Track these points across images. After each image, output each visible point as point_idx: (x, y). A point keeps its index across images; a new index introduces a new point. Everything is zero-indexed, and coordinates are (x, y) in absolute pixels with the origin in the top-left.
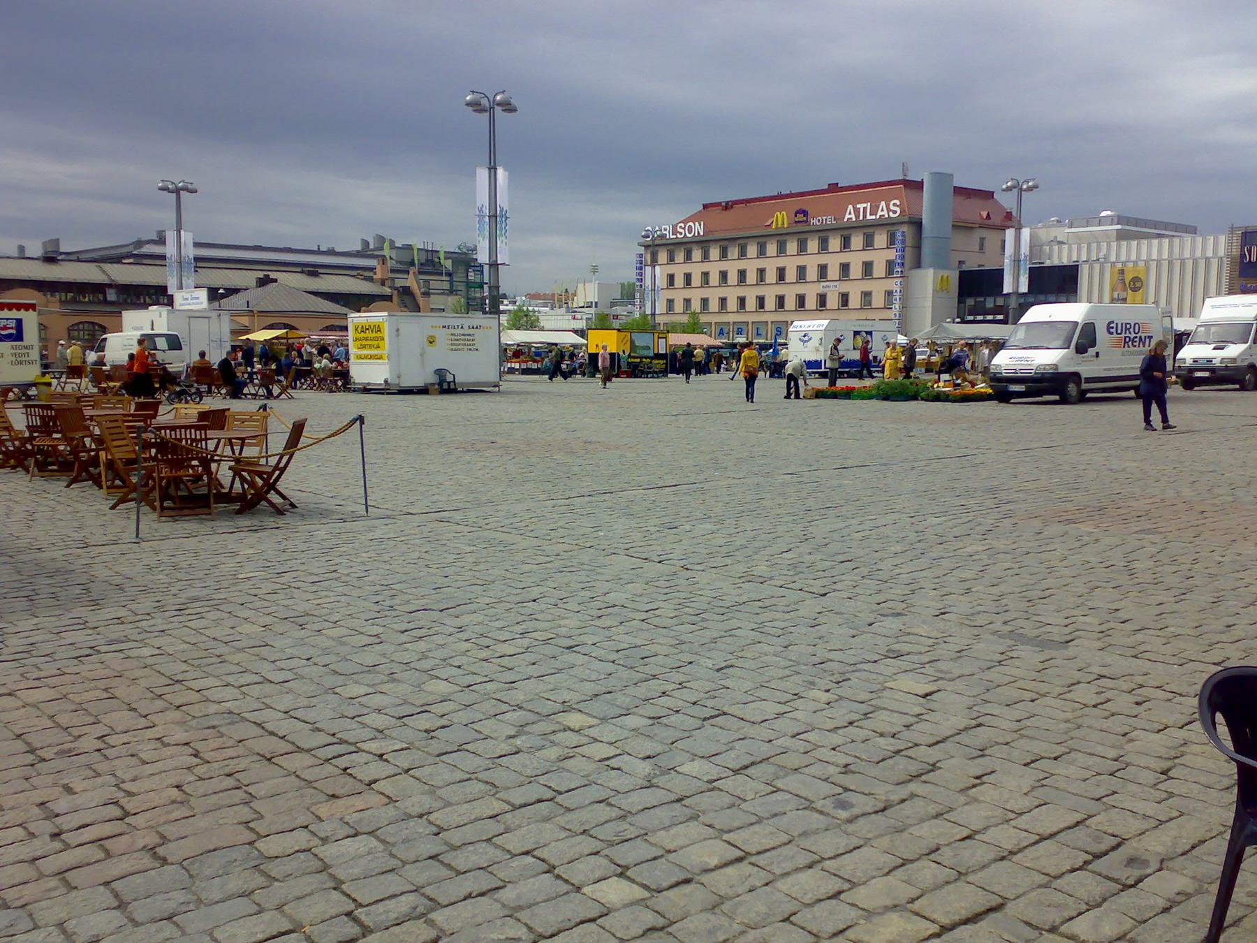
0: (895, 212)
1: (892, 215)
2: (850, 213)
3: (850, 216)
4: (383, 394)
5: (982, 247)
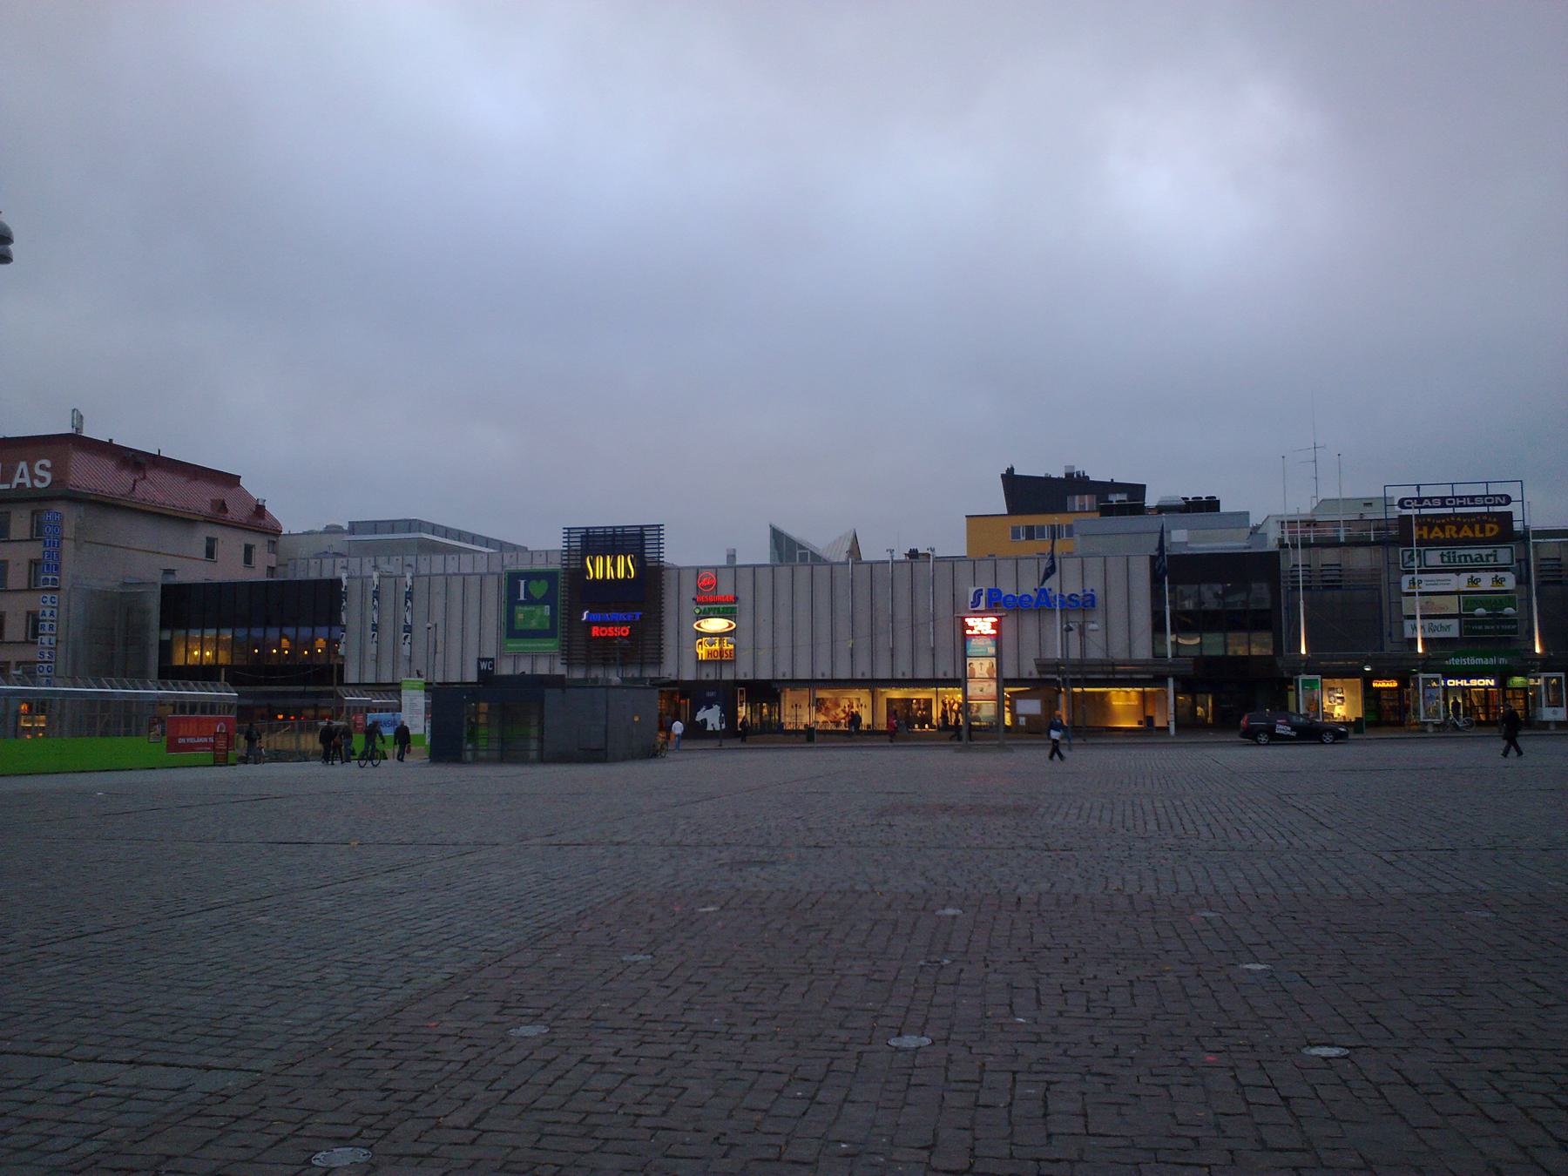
0: (42, 479)
1: (38, 484)
2: (22, 476)
3: (21, 481)
4: (944, 561)
5: (210, 553)
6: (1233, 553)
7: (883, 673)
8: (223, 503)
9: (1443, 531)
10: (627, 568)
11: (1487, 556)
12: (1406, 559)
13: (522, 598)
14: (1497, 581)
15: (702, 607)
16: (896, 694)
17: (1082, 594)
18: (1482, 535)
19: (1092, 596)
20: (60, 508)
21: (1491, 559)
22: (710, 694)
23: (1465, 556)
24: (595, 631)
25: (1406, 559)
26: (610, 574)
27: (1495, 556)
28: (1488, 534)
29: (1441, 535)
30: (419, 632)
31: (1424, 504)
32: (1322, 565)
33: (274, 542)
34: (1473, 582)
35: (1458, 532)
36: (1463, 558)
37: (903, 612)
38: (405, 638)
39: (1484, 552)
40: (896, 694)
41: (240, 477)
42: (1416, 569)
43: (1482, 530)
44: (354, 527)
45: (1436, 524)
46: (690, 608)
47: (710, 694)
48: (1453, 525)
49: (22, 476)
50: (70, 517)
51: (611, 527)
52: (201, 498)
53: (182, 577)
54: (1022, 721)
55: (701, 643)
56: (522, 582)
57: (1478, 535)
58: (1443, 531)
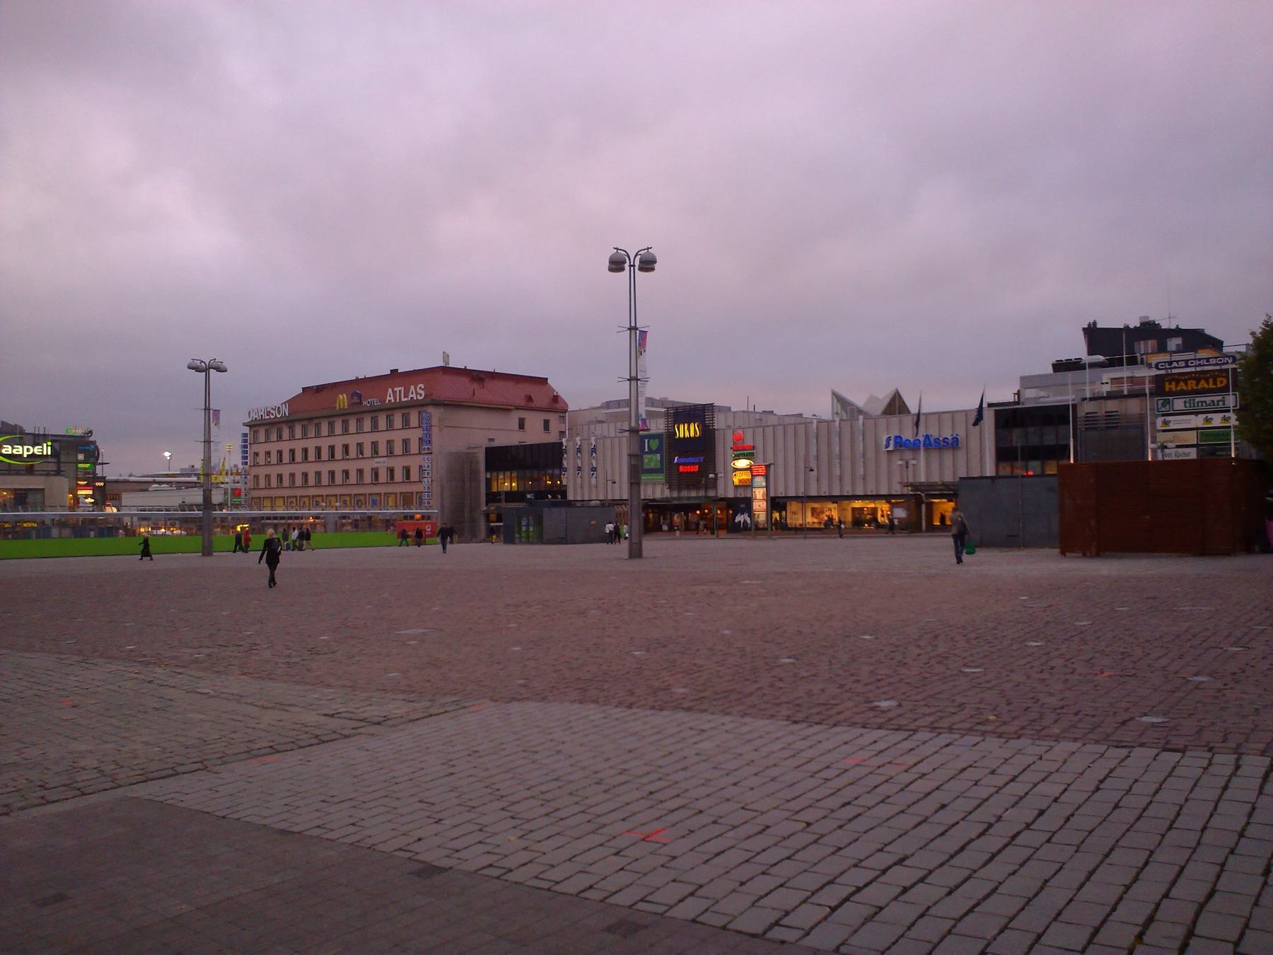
1: (420, 398)
2: (390, 396)
6: (1041, 407)
7: (847, 491)
8: (530, 396)
9: (1186, 384)
10: (695, 430)
11: (1218, 401)
12: (1160, 406)
13: (646, 450)
14: (1165, 424)
15: (736, 453)
16: (858, 504)
17: (952, 437)
18: (1214, 387)
19: (957, 438)
20: (430, 410)
21: (1221, 403)
22: (743, 506)
23: (1202, 402)
24: (681, 468)
25: (1160, 406)
26: (687, 435)
27: (1224, 401)
28: (1219, 385)
29: (1185, 388)
30: (600, 470)
31: (1173, 366)
32: (1106, 412)
33: (563, 417)
34: (1208, 420)
35: (1197, 385)
36: (1200, 404)
37: (847, 453)
38: (593, 474)
39: (1216, 399)
40: (858, 504)
41: (547, 379)
42: (1231, 409)
43: (1215, 383)
44: (608, 405)
45: (1181, 380)
46: (731, 453)
47: (743, 506)
48: (1193, 380)
49: (390, 396)
50: (435, 414)
51: (12, 475)
52: (517, 394)
53: (496, 444)
54: (896, 522)
55: (735, 475)
56: (646, 441)
57: (1211, 386)
58: (1186, 384)
